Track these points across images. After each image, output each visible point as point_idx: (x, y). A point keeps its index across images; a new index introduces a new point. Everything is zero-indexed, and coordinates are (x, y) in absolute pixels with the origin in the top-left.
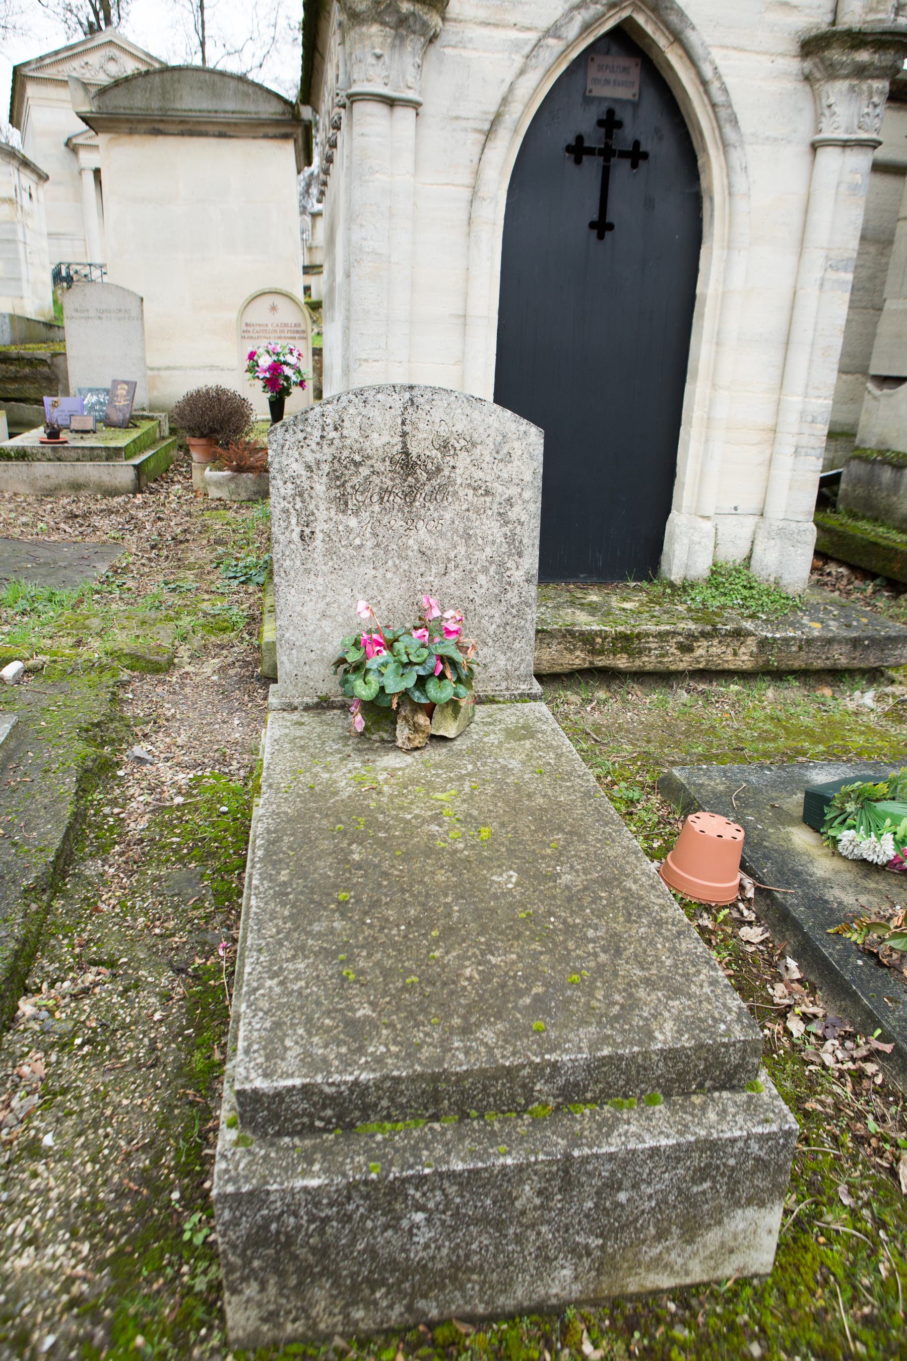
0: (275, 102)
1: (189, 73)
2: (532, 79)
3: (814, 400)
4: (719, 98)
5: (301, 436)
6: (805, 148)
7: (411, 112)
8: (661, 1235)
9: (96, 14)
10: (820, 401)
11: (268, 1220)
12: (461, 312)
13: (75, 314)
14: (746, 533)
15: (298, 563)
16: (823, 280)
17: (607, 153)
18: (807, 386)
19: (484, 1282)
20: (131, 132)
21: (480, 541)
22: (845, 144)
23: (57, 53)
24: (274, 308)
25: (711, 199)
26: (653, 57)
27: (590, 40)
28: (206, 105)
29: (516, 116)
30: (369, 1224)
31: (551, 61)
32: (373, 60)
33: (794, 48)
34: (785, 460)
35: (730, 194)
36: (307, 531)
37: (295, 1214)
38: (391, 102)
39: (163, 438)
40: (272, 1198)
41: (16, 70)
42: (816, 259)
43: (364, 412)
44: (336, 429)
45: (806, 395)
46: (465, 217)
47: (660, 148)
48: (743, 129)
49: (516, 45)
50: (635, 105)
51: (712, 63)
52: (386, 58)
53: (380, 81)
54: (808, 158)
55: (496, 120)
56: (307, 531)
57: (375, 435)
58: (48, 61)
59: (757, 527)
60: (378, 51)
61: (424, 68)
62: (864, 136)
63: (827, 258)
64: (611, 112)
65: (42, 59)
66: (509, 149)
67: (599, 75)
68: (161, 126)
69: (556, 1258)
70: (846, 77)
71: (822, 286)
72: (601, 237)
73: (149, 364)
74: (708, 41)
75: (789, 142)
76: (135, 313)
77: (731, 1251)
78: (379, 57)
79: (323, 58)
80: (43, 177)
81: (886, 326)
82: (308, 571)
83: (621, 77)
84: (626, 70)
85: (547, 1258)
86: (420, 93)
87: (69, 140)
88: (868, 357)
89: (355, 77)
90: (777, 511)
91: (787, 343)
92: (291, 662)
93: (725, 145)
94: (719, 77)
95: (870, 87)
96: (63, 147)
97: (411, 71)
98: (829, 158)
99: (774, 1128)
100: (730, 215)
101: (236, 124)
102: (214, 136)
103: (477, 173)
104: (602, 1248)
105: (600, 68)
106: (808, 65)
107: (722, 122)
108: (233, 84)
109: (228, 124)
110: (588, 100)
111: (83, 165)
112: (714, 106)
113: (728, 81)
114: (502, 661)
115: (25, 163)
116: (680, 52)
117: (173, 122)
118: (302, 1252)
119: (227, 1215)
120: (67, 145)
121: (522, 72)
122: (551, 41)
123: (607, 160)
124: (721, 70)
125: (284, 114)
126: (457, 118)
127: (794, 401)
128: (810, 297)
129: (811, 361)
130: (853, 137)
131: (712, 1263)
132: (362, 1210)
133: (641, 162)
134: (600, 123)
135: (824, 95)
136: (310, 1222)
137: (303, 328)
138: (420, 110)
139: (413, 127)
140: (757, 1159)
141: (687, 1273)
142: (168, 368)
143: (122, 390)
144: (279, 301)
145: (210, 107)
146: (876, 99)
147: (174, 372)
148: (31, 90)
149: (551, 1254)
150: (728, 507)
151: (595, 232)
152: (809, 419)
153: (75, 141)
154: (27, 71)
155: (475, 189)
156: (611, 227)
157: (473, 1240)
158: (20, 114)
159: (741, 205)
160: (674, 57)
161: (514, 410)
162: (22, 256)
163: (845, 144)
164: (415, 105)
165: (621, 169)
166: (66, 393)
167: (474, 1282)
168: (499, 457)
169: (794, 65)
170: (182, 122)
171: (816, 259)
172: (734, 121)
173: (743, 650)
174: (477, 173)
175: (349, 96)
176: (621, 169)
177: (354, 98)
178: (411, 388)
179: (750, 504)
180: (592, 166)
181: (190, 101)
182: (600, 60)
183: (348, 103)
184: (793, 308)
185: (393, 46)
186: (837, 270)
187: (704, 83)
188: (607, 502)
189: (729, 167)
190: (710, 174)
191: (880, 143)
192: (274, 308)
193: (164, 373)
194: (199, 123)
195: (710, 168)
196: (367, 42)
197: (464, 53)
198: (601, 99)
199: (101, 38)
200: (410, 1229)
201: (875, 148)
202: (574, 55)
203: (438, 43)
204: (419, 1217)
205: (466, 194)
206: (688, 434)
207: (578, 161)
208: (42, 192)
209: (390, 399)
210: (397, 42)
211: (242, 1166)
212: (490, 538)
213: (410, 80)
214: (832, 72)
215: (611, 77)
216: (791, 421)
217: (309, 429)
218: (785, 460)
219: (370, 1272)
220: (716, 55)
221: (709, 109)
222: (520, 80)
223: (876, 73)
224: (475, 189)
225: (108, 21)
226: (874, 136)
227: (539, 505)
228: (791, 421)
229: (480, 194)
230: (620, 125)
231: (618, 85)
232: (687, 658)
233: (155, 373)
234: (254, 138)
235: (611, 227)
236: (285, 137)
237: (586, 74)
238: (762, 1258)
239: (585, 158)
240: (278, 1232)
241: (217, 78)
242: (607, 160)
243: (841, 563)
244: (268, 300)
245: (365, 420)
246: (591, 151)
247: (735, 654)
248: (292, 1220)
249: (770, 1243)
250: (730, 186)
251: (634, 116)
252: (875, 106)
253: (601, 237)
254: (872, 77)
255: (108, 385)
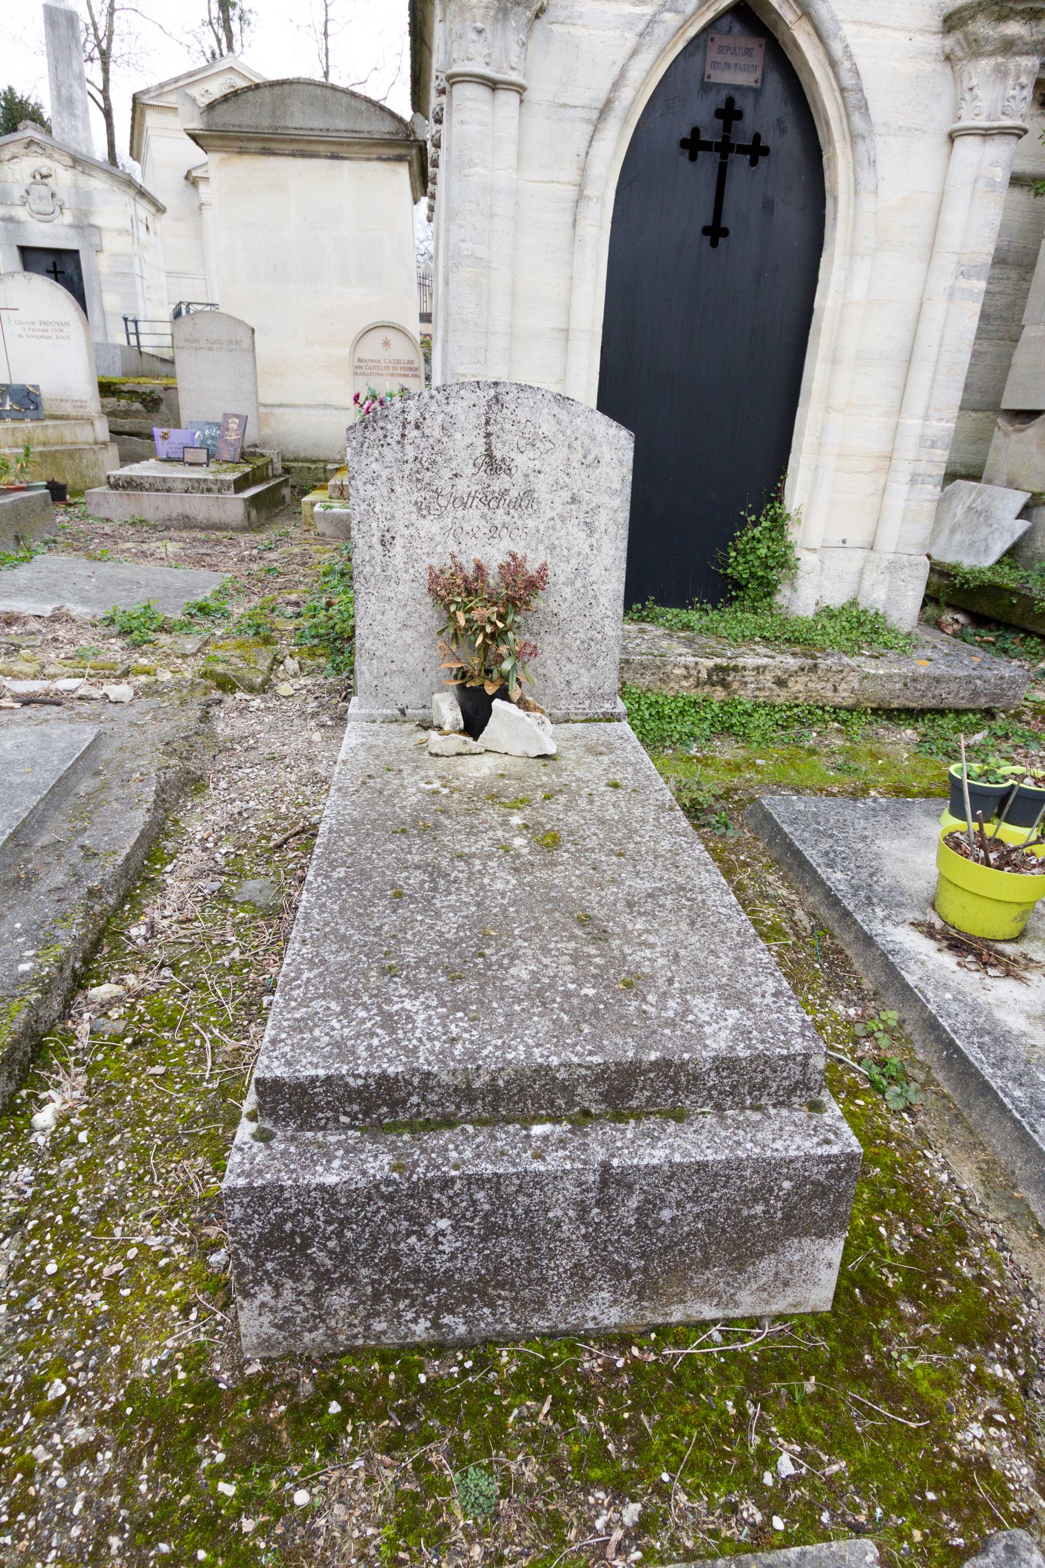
0: (388, 120)
1: (301, 87)
2: (645, 60)
3: (934, 423)
4: (848, 81)
5: (380, 433)
6: (943, 139)
7: (513, 98)
8: (706, 1263)
9: (219, 41)
10: (942, 424)
11: (282, 1219)
12: (563, 326)
13: (186, 344)
14: (854, 566)
15: (378, 570)
16: (952, 287)
17: (725, 148)
18: (928, 408)
19: (515, 1299)
20: (242, 152)
21: (565, 552)
22: (986, 134)
23: (176, 80)
24: (386, 343)
25: (835, 199)
26: (778, 36)
27: (710, 15)
28: (318, 123)
29: (626, 102)
30: (391, 1229)
31: (666, 39)
32: (473, 36)
33: (937, 23)
34: (900, 488)
35: (856, 192)
36: (388, 536)
37: (311, 1213)
38: (493, 85)
39: (275, 476)
40: (287, 1195)
41: (135, 98)
42: (946, 262)
43: (449, 409)
44: (417, 427)
45: (926, 417)
46: (570, 221)
47: (784, 144)
48: (873, 118)
49: (629, 22)
50: (757, 92)
51: (843, 40)
52: (488, 33)
53: (481, 60)
54: (945, 150)
55: (605, 110)
56: (388, 536)
57: (458, 436)
58: (166, 89)
59: (866, 561)
60: (479, 25)
61: (531, 46)
62: (1007, 122)
63: (959, 263)
64: (730, 101)
65: (161, 86)
66: (619, 141)
67: (720, 58)
68: (273, 146)
69: (594, 1277)
70: (992, 54)
71: (951, 295)
72: (714, 244)
73: (261, 400)
74: (840, 15)
75: (924, 132)
76: (246, 343)
77: (786, 1284)
78: (480, 32)
79: (430, 52)
80: (160, 209)
81: (1022, 356)
82: (388, 578)
83: (743, 60)
84: (748, 52)
85: (583, 1277)
86: (525, 76)
87: (189, 172)
88: (1000, 392)
89: (455, 55)
90: (887, 544)
91: (910, 361)
92: (371, 673)
93: (854, 137)
94: (850, 57)
95: (1018, 66)
96: (183, 181)
97: (515, 48)
98: (968, 149)
99: (835, 1150)
100: (855, 216)
101: (348, 144)
102: (326, 157)
103: (584, 170)
104: (645, 1270)
105: (721, 49)
106: (950, 42)
107: (851, 109)
108: (345, 99)
109: (341, 144)
110: (706, 87)
111: (203, 200)
112: (842, 90)
113: (861, 62)
114: (585, 680)
115: (142, 193)
116: (809, 28)
117: (283, 141)
118: (321, 1256)
119: (238, 1212)
120: (186, 178)
121: (635, 53)
122: (667, 16)
123: (724, 156)
124: (854, 50)
125: (397, 133)
126: (565, 105)
127: (913, 423)
128: (936, 312)
129: (934, 380)
130: (996, 124)
131: (765, 1295)
132: (383, 1212)
133: (761, 158)
134: (719, 114)
135: (966, 76)
136: (327, 1223)
137: (416, 365)
138: (525, 94)
139: (516, 115)
140: (816, 1184)
141: (737, 1305)
142: (281, 406)
143: (234, 424)
144: (391, 335)
145: (322, 126)
146: (1023, 80)
147: (288, 410)
148: (151, 119)
149: (589, 1273)
150: (835, 539)
151: (687, 153)
152: (929, 443)
153: (194, 174)
154: (145, 99)
155: (581, 187)
156: (725, 233)
157: (504, 1251)
158: (139, 147)
159: (867, 203)
160: (802, 36)
161: (611, 416)
162: (139, 291)
163: (986, 134)
164: (520, 89)
165: (739, 164)
166: (178, 425)
167: (506, 1299)
168: (586, 462)
169: (935, 43)
170: (292, 141)
171: (946, 262)
172: (864, 108)
173: (844, 686)
174: (584, 170)
175: (449, 78)
176: (739, 164)
177: (454, 79)
178: (496, 384)
179: (858, 536)
180: (708, 161)
181: (300, 118)
182: (720, 40)
183: (447, 86)
184: (918, 322)
185: (496, 19)
186: (969, 277)
187: (833, 64)
188: (703, 513)
189: (856, 163)
190: (836, 171)
191: (1025, 131)
192: (386, 343)
193: (278, 411)
194: (310, 142)
195: (835, 165)
196: (468, 15)
197: (573, 30)
198: (720, 86)
199: (223, 64)
200: (436, 1236)
201: (1020, 137)
202: (692, 32)
203: (544, 18)
204: (444, 1224)
205: (571, 193)
206: (797, 461)
207: (693, 158)
208: (161, 224)
209: (474, 396)
210: (500, 16)
211: (258, 1159)
212: (575, 549)
213: (514, 60)
214: (975, 49)
215: (732, 60)
216: (909, 448)
217: (389, 427)
218: (900, 488)
219: (393, 1281)
220: (848, 31)
221: (837, 94)
222: (632, 62)
223: (1026, 48)
224: (581, 187)
225: (230, 47)
226: (1018, 122)
227: (627, 514)
228: (909, 448)
229: (586, 193)
230: (739, 115)
231: (739, 71)
232: (784, 693)
233: (269, 410)
234: (368, 159)
235: (725, 233)
236: (399, 159)
237: (705, 56)
238: (821, 1295)
239: (700, 153)
240: (293, 1233)
241: (328, 92)
242: (724, 156)
243: (957, 609)
244: (381, 335)
245: (448, 419)
246: (707, 146)
247: (835, 690)
248: (307, 1220)
249: (829, 1279)
250: (856, 182)
251: (756, 104)
252: (1023, 87)
253: (714, 244)
254: (1021, 54)
255: (219, 419)
